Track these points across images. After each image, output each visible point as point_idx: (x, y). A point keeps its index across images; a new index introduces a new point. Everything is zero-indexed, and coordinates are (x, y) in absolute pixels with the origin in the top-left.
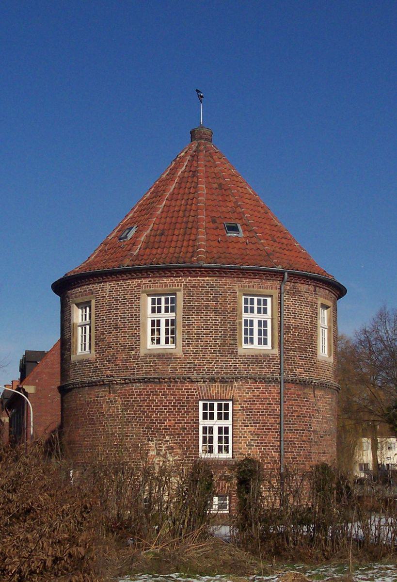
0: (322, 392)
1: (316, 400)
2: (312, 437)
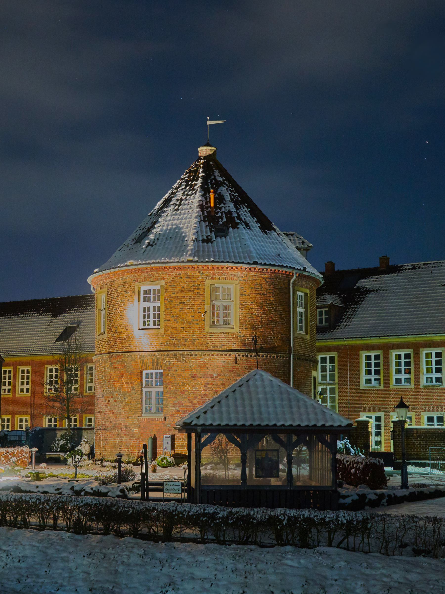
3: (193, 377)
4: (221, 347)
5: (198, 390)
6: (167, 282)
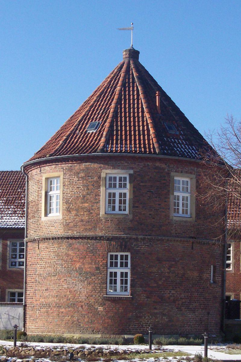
0: (46, 245)
1: (40, 251)
2: (37, 279)
3: (159, 260)
4: (182, 234)
5: (163, 273)
6: (136, 171)
